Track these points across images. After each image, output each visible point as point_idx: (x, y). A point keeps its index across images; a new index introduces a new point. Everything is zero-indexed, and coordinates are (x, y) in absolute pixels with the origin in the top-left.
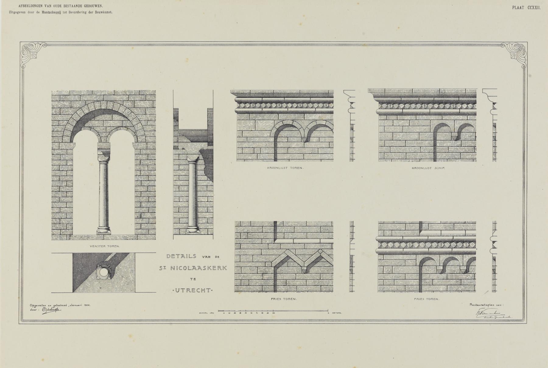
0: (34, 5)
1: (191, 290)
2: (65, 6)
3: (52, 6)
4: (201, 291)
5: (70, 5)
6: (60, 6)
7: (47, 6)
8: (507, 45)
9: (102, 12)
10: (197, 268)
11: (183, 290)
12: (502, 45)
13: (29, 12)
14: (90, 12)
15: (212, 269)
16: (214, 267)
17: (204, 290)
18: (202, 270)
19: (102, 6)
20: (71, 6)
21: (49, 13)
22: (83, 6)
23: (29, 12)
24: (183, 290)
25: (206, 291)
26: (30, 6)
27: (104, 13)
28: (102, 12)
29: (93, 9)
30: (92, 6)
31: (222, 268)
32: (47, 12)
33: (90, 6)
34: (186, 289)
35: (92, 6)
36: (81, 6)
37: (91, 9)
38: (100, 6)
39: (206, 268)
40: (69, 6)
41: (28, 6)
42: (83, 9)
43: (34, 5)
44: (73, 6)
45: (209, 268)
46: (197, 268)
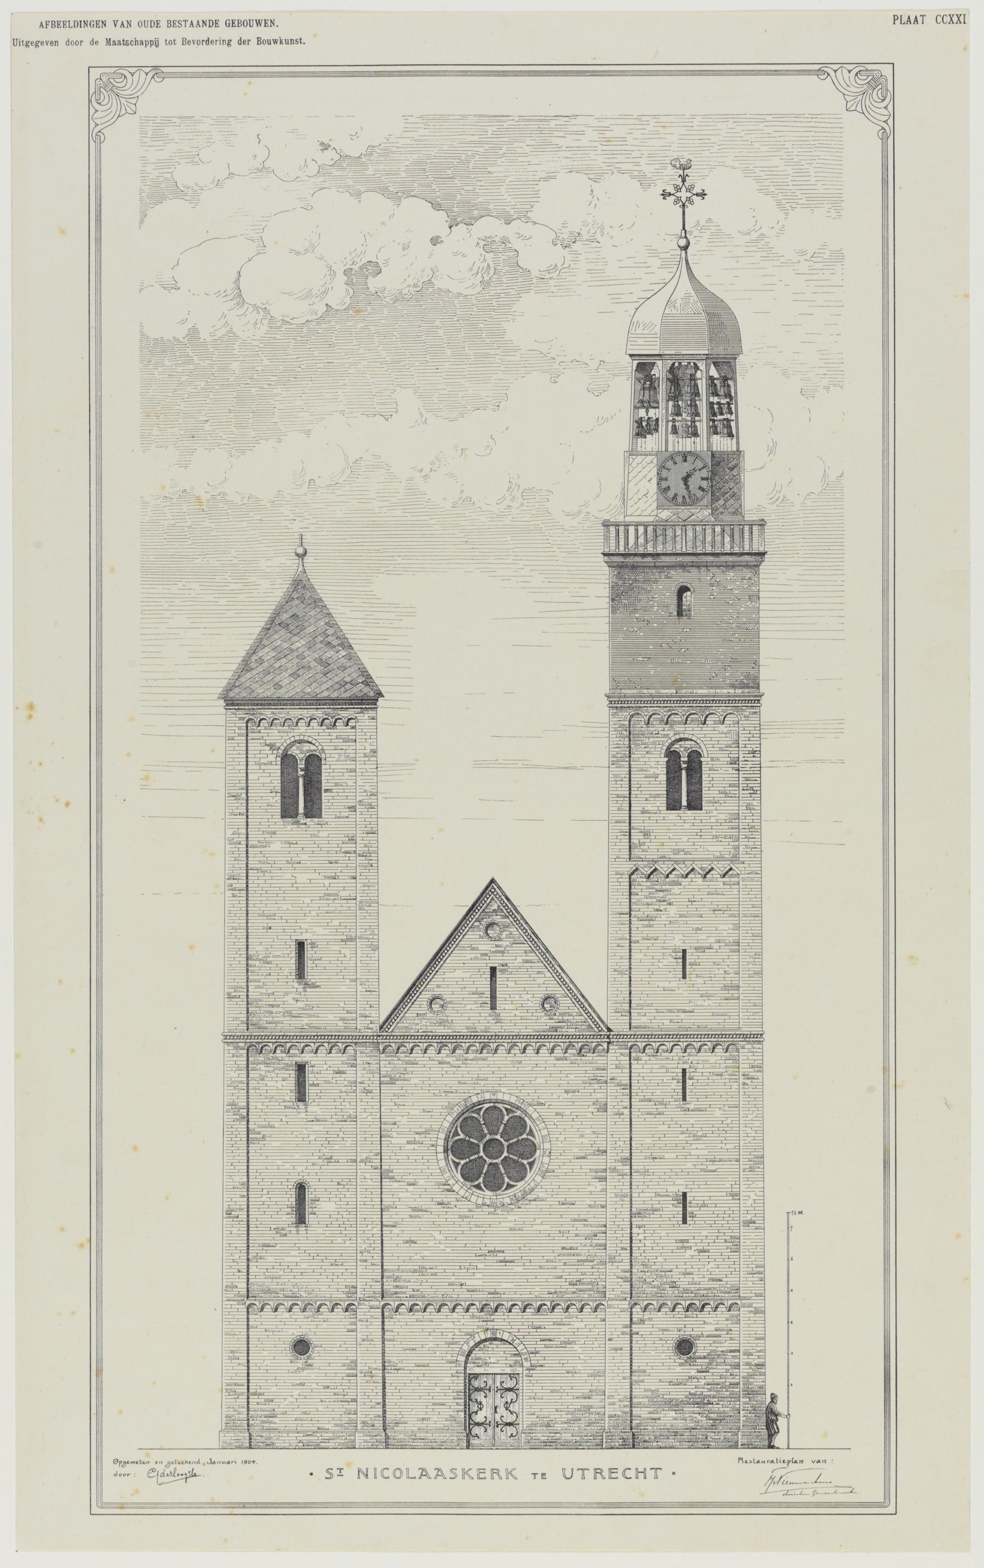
0: (83, 23)
1: (606, 1473)
2: (171, 24)
3: (134, 24)
4: (633, 1477)
5: (185, 21)
6: (157, 24)
7: (119, 24)
8: (835, 71)
9: (275, 42)
10: (432, 1473)
11: (583, 1474)
12: (820, 71)
13: (68, 43)
14: (241, 42)
15: (475, 1477)
16: (481, 1471)
17: (644, 1472)
18: (448, 1478)
19: (276, 25)
20: (188, 24)
21: (126, 43)
22: (222, 24)
23: (68, 43)
24: (583, 1474)
25: (650, 1474)
26: (72, 24)
27: (281, 42)
28: (275, 42)
29: (251, 33)
30: (248, 23)
31: (503, 1474)
32: (119, 41)
33: (241, 23)
34: (592, 1472)
35: (248, 23)
36: (216, 23)
37: (245, 33)
38: (269, 23)
39: (459, 1473)
40: (183, 23)
41: (67, 24)
42: (223, 32)
43: (83, 23)
44: (195, 24)
45: (465, 1473)
46: (432, 1473)
